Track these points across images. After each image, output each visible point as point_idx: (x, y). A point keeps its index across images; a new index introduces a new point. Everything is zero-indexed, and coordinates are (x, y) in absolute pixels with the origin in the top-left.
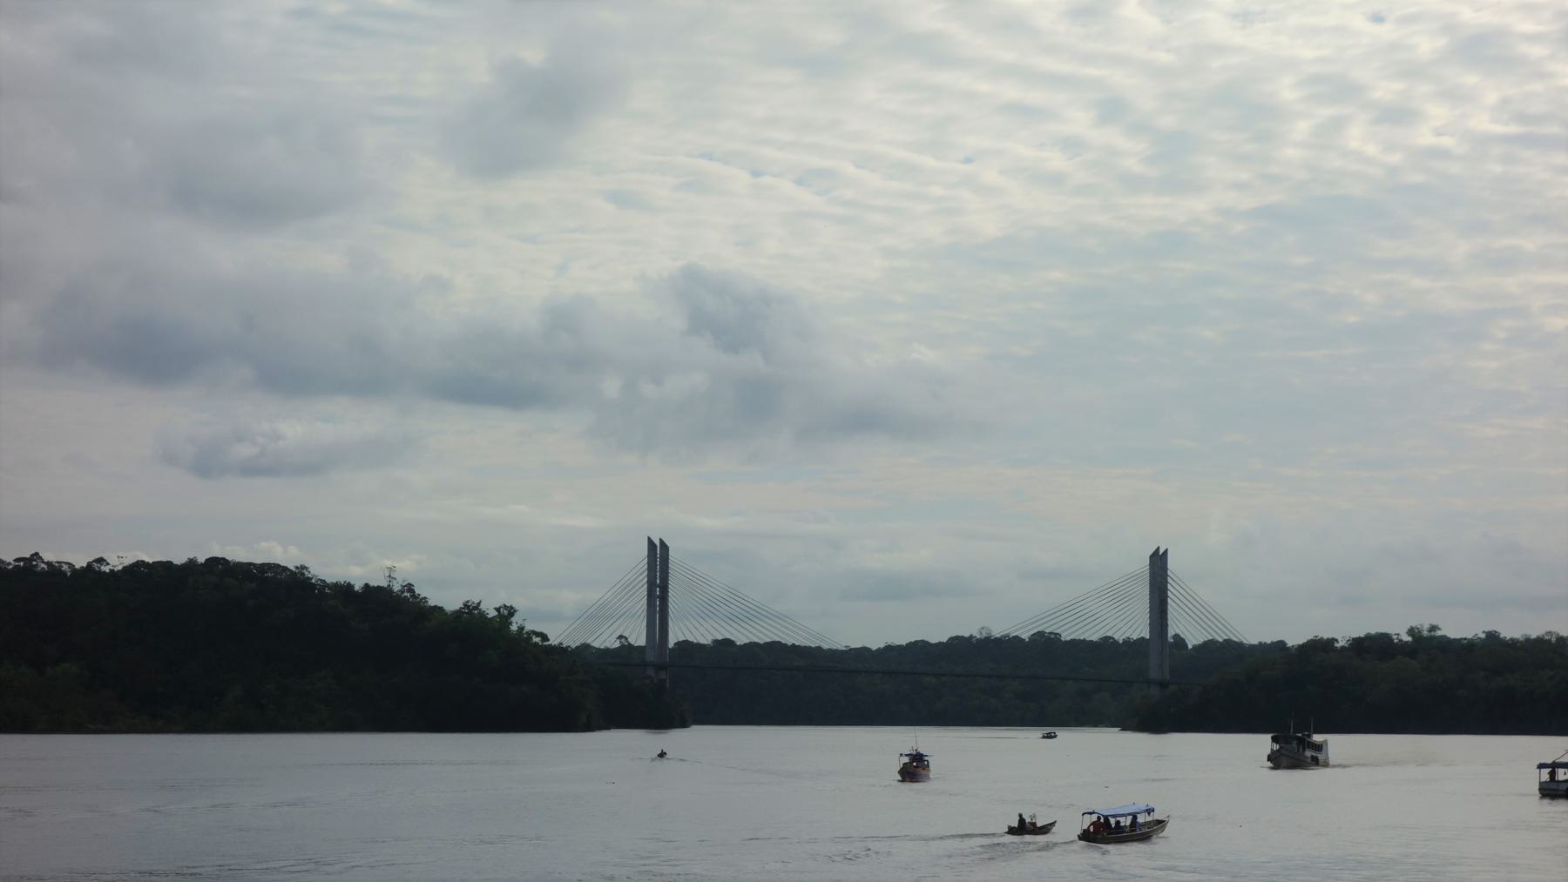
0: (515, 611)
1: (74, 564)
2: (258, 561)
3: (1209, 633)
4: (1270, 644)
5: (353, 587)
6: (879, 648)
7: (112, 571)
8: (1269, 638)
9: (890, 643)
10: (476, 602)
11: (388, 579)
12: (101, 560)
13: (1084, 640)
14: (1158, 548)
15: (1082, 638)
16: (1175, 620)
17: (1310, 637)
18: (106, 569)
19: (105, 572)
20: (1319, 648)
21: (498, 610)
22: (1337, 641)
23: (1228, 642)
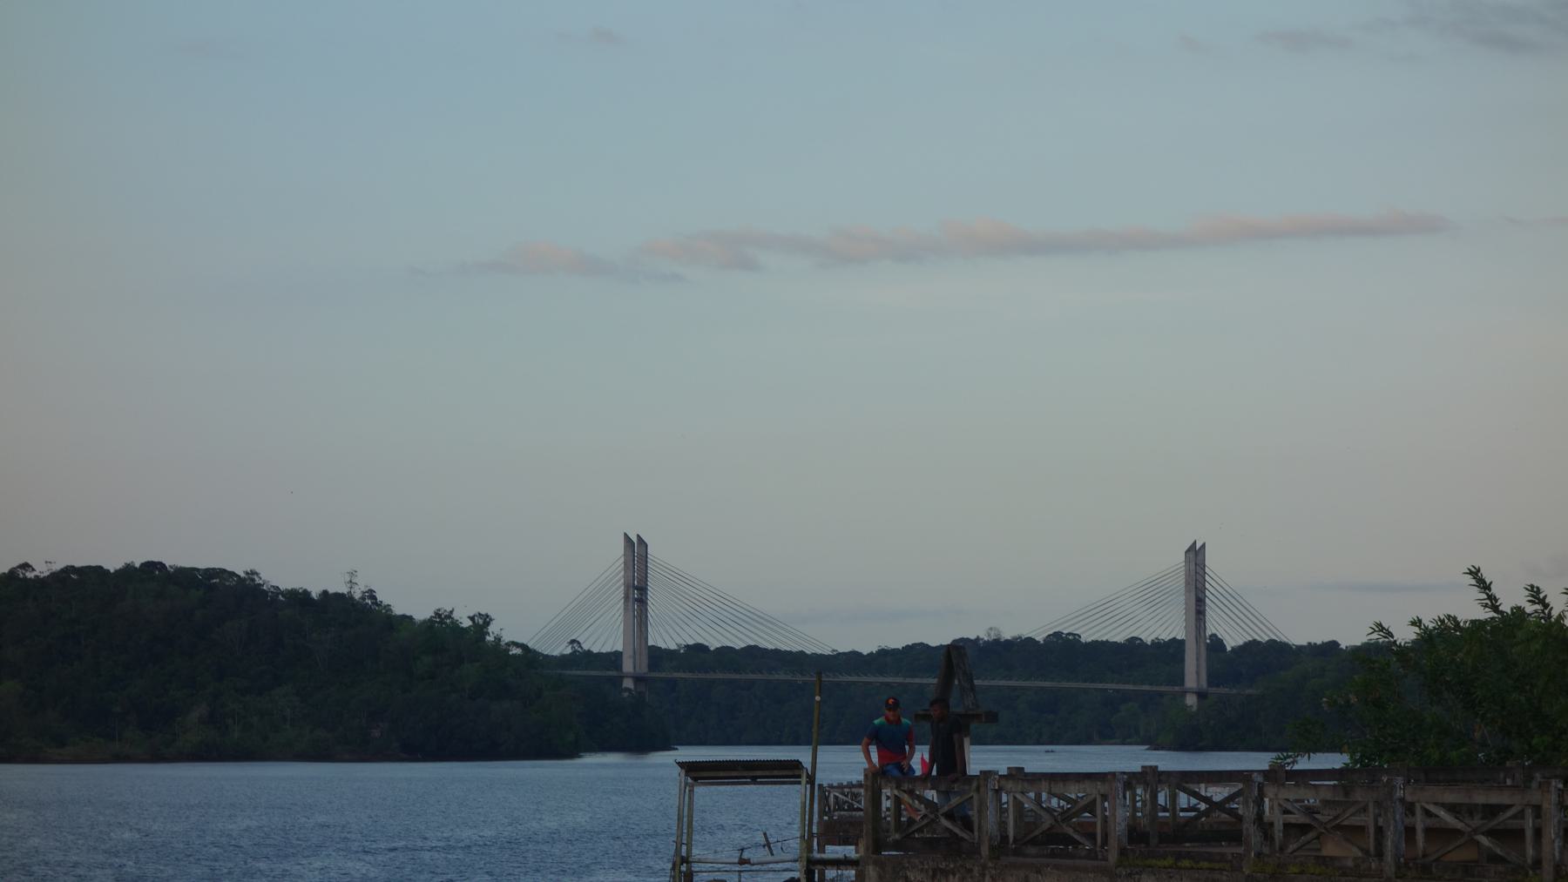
0: (491, 620)
2: (202, 565)
3: (741, 640)
4: (1320, 645)
6: (872, 653)
7: (37, 576)
8: (850, 650)
9: (883, 647)
10: (449, 609)
11: (349, 585)
12: (26, 566)
13: (1107, 641)
14: (1195, 542)
15: (1104, 639)
16: (1213, 622)
18: (30, 575)
19: (30, 579)
21: (472, 618)
23: (1272, 642)
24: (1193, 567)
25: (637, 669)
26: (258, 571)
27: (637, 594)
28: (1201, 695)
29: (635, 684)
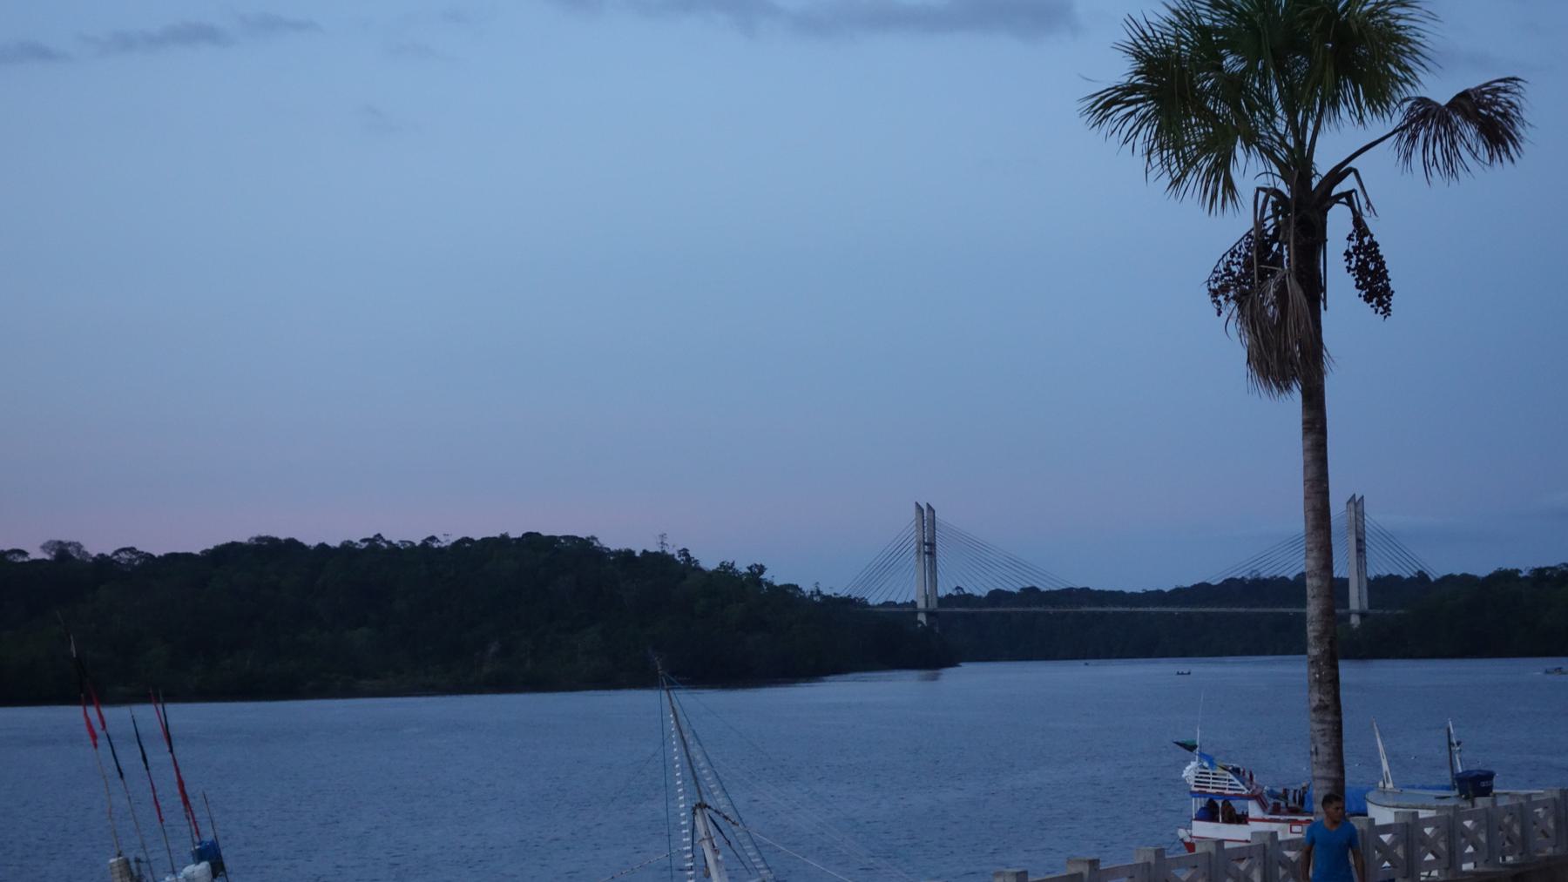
1: (414, 541)
5: (633, 553)
7: (439, 548)
8: (1173, 587)
10: (731, 562)
12: (433, 538)
14: (1354, 495)
17: (582, 533)
18: (436, 545)
20: (1504, 578)
21: (750, 568)
22: (1521, 572)
24: (1353, 514)
25: (930, 606)
26: (596, 536)
27: (929, 549)
28: (1363, 615)
29: (927, 618)
